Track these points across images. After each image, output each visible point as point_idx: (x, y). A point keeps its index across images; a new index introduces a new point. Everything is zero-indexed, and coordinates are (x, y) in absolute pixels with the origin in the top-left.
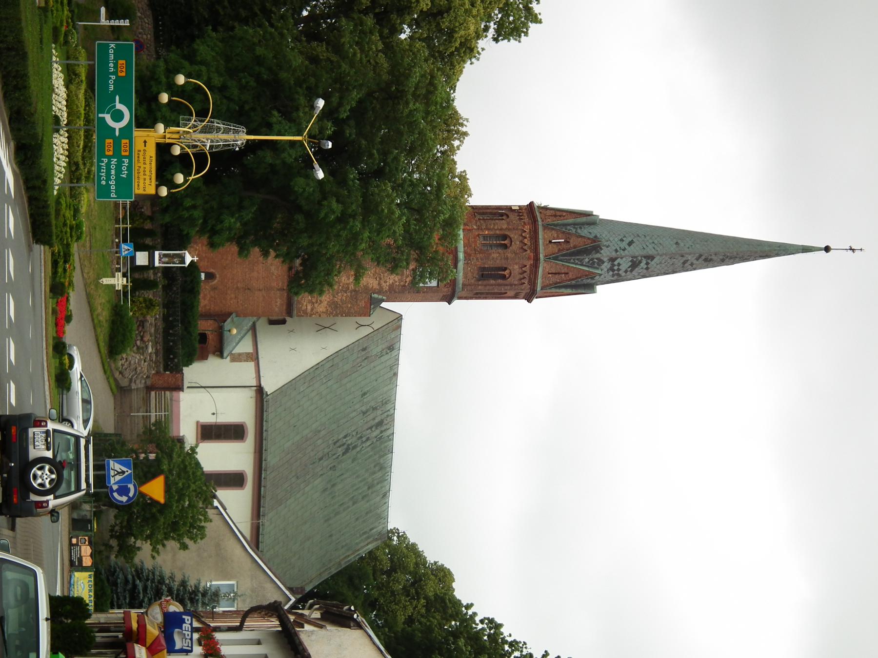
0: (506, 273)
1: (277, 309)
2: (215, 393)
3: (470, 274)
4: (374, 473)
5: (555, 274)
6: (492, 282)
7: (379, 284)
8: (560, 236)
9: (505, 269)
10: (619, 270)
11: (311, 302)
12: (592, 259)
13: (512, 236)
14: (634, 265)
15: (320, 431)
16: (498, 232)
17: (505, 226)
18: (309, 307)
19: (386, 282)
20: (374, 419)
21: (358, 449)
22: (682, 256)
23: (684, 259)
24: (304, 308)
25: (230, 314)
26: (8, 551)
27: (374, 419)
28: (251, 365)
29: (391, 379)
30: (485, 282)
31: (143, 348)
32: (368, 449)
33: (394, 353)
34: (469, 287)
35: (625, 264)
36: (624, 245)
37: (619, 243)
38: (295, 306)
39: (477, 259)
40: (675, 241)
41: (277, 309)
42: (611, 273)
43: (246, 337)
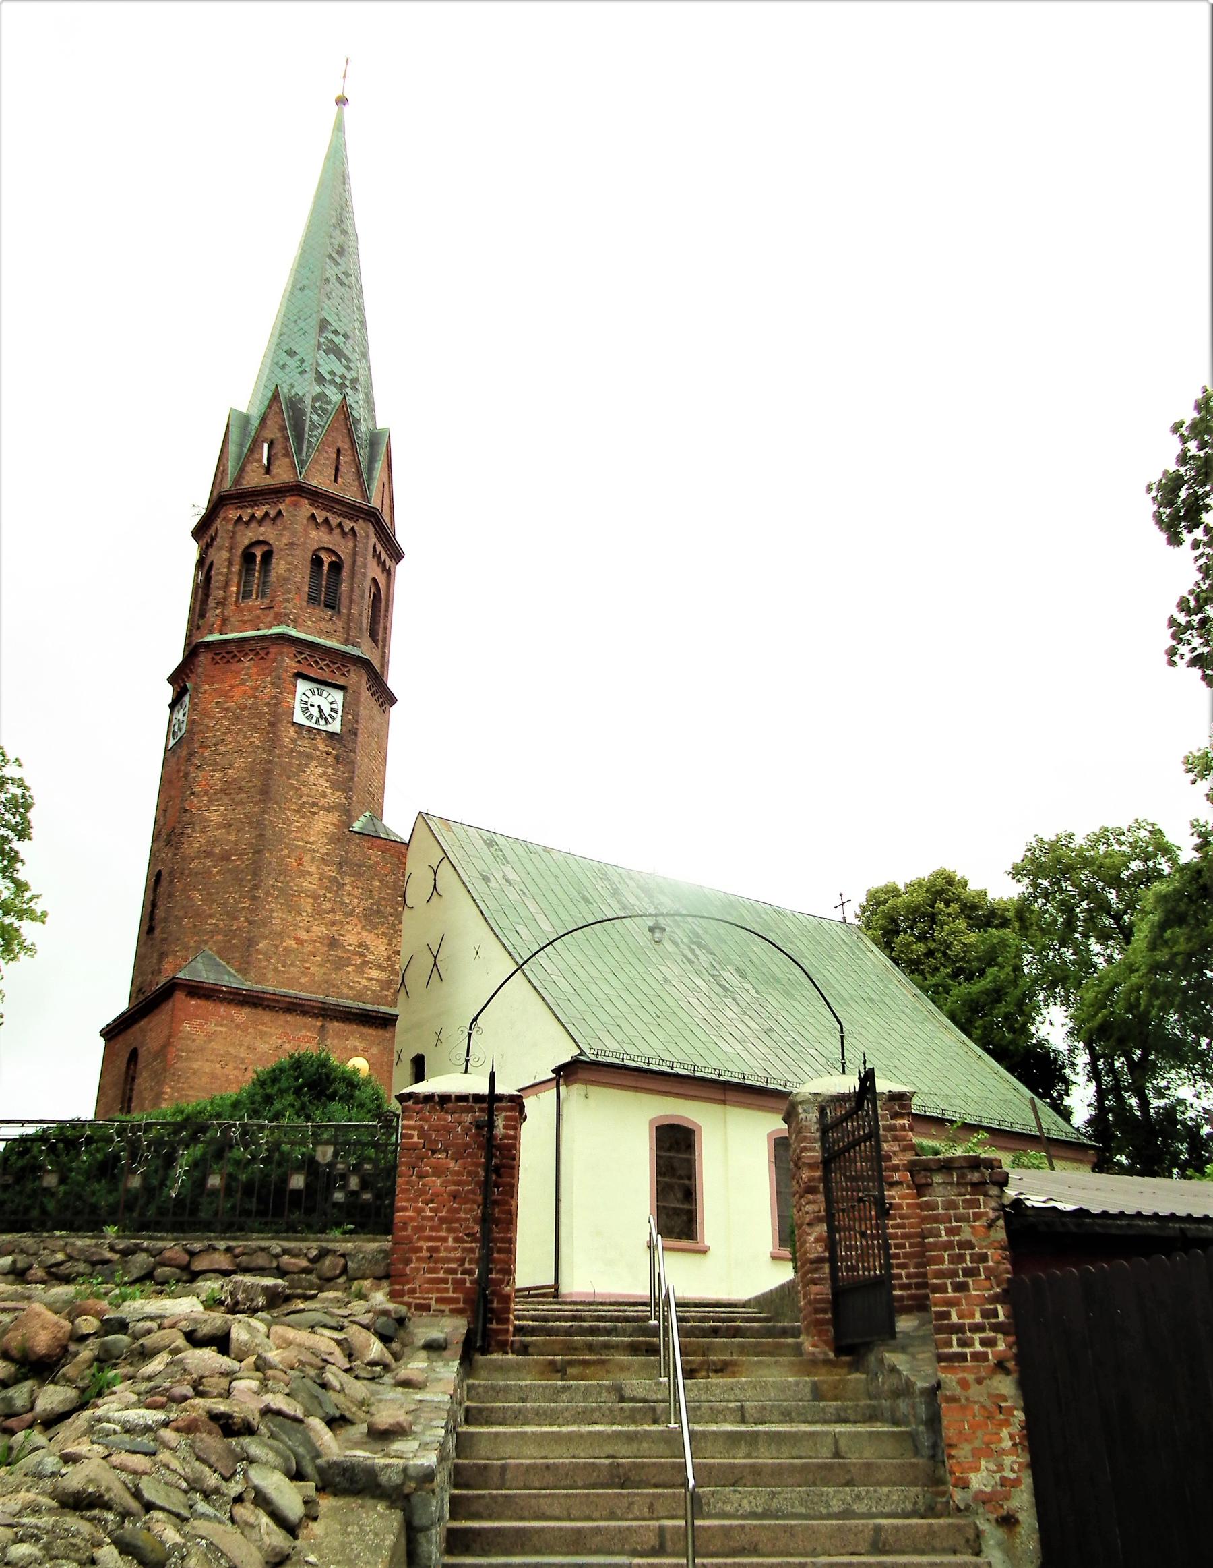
0: (327, 559)
5: (337, 470)
6: (344, 587)
7: (328, 809)
10: (343, 377)
12: (313, 407)
13: (247, 542)
14: (335, 351)
16: (235, 568)
17: (225, 555)
18: (375, 974)
23: (333, 279)
24: (375, 986)
30: (344, 600)
33: (501, 841)
34: (353, 633)
35: (329, 365)
37: (287, 370)
38: (369, 1007)
39: (286, 600)
40: (298, 292)
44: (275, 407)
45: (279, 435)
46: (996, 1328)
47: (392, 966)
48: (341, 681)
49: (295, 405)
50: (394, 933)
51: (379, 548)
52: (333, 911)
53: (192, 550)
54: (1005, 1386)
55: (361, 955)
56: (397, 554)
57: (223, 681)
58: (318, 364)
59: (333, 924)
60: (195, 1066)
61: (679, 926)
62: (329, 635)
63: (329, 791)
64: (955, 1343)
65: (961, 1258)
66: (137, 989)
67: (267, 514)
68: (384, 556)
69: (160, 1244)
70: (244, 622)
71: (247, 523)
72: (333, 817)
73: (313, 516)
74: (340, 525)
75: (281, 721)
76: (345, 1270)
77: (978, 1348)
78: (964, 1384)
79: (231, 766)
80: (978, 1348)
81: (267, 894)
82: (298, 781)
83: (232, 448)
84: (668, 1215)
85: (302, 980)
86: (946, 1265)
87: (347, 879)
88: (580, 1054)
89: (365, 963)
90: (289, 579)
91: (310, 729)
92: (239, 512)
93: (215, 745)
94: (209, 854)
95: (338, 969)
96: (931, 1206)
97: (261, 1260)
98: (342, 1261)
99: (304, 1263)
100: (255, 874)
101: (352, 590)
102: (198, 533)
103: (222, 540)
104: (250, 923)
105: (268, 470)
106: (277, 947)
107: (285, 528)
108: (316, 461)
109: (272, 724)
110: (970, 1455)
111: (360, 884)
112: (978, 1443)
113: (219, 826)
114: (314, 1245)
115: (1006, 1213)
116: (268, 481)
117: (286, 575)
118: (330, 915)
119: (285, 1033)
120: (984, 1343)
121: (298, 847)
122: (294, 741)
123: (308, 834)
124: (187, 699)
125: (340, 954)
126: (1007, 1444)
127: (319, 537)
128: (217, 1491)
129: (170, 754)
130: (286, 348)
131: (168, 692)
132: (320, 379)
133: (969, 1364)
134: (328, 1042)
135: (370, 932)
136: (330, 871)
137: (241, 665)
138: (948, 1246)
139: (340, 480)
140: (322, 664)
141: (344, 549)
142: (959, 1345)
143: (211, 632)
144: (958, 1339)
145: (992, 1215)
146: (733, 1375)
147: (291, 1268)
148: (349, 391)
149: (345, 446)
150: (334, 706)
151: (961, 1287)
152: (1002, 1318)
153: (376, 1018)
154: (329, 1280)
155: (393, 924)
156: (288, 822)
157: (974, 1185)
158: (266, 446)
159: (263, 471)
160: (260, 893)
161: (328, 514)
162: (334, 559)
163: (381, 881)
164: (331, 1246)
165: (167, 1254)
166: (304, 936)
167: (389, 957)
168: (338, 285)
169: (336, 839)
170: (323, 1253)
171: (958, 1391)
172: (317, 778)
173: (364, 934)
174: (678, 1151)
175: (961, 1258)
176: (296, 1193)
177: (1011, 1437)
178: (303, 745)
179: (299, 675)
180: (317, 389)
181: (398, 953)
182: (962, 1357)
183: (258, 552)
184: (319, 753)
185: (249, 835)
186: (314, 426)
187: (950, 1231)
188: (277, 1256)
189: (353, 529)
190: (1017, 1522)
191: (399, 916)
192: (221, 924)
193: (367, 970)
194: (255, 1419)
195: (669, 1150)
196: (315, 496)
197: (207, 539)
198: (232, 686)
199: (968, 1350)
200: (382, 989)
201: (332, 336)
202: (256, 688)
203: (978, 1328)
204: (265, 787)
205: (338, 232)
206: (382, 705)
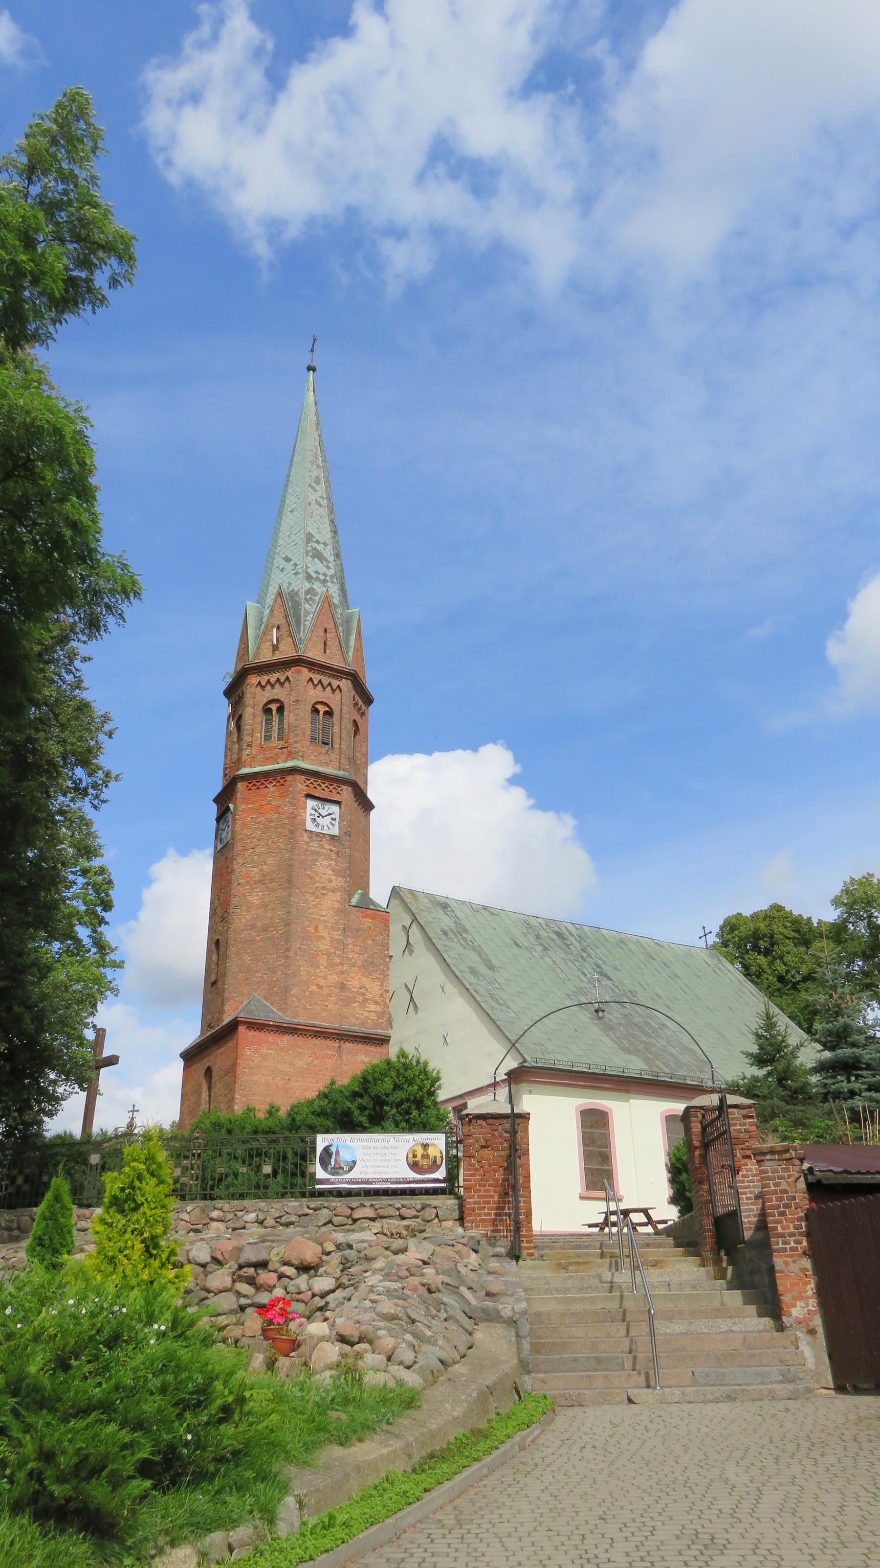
0: (322, 709)
3: (322, 757)
4: (630, 950)
6: (336, 729)
7: (333, 891)
8: (268, 638)
9: (315, 711)
10: (325, 575)
12: (306, 599)
13: (265, 701)
17: (259, 735)
18: (373, 1007)
19: (330, 881)
20: (553, 940)
21: (600, 962)
23: (313, 503)
24: (373, 1016)
29: (492, 914)
30: (337, 740)
31: (345, 1265)
32: (598, 952)
33: (452, 904)
36: (289, 567)
37: (285, 572)
38: (370, 1031)
39: (296, 742)
45: (284, 621)
46: (801, 1234)
49: (294, 595)
50: (384, 978)
51: (357, 698)
54: (807, 1263)
55: (364, 994)
58: (307, 567)
60: (255, 1078)
63: (333, 878)
65: (781, 1199)
66: (207, 1024)
68: (360, 703)
69: (334, 1204)
70: (268, 759)
73: (311, 679)
74: (330, 684)
75: (297, 829)
77: (793, 1244)
80: (793, 1244)
81: (296, 954)
84: (592, 1175)
85: (324, 1015)
86: (774, 1203)
87: (350, 941)
89: (365, 1000)
90: (296, 727)
91: (318, 834)
92: (258, 679)
94: (253, 927)
96: (766, 1172)
97: (392, 1211)
98: (435, 1211)
100: (287, 941)
102: (228, 693)
103: (248, 699)
104: (286, 975)
106: (305, 991)
109: (292, 832)
112: (795, 1293)
114: (418, 1202)
115: (805, 1174)
116: (278, 656)
117: (296, 723)
119: (314, 1053)
120: (796, 1242)
122: (307, 843)
123: (321, 910)
125: (347, 994)
126: (810, 1293)
127: (316, 694)
128: (437, 1316)
130: (283, 556)
131: (214, 809)
132: (309, 578)
134: (344, 1057)
136: (337, 935)
138: (775, 1192)
139: (328, 651)
140: (323, 786)
141: (334, 701)
143: (245, 767)
145: (797, 1175)
146: (662, 1267)
148: (329, 584)
151: (782, 1214)
155: (383, 971)
157: (787, 1160)
158: (275, 630)
160: (291, 954)
162: (327, 709)
163: (373, 940)
164: (428, 1202)
165: (339, 1210)
166: (322, 982)
167: (382, 995)
168: (317, 507)
169: (341, 912)
172: (326, 870)
173: (364, 979)
174: (597, 1128)
177: (812, 1289)
178: (314, 846)
179: (308, 796)
180: (307, 586)
182: (785, 1250)
183: (274, 707)
184: (325, 851)
186: (307, 613)
187: (776, 1185)
188: (398, 1209)
189: (339, 687)
190: (816, 1332)
191: (386, 965)
193: (367, 1005)
194: (440, 1285)
195: (591, 1127)
196: (312, 665)
198: (262, 806)
201: (315, 545)
203: (792, 1235)
204: (287, 878)
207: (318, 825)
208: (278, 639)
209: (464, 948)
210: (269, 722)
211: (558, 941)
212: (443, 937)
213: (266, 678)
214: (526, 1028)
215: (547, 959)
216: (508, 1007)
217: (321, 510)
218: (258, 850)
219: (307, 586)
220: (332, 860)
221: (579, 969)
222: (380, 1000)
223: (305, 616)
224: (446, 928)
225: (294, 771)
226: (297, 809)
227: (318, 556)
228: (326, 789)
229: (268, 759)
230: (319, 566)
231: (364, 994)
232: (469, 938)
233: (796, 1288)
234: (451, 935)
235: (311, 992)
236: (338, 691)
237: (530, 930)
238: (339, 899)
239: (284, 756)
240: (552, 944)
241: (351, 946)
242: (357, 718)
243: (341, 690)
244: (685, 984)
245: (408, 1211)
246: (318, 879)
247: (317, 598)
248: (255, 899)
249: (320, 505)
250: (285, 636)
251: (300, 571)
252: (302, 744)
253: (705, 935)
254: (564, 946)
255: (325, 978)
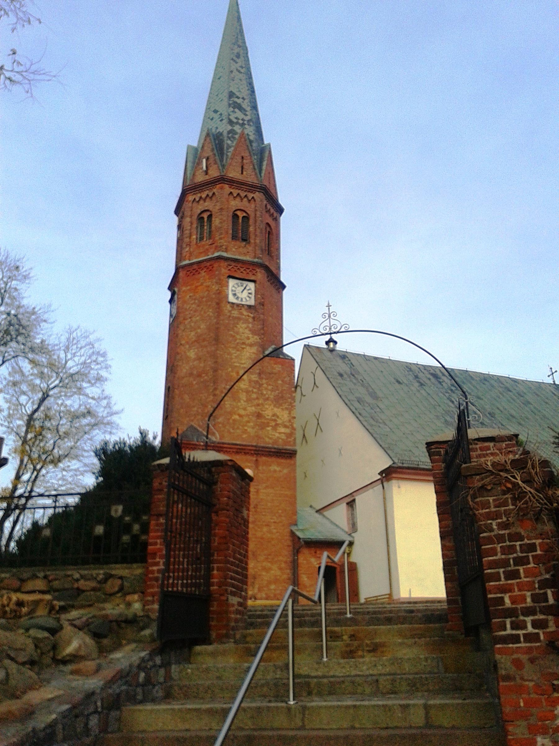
0: (241, 214)
1: (285, 471)
2: (312, 335)
3: (241, 250)
6: (251, 229)
7: (251, 345)
9: (235, 216)
10: (243, 120)
11: (275, 428)
13: (199, 212)
15: (446, 421)
16: (195, 226)
18: (282, 430)
19: (248, 338)
20: (429, 379)
22: (232, 72)
23: (235, 71)
24: (283, 437)
25: (293, 534)
26: (259, 648)
27: (429, 379)
28: (358, 499)
30: (252, 236)
36: (216, 116)
37: (214, 120)
38: (281, 447)
39: (221, 239)
41: (285, 471)
42: (246, 126)
43: (328, 517)
44: (208, 140)
46: (547, 610)
47: (292, 425)
48: (253, 278)
50: (291, 408)
52: (257, 398)
53: (175, 220)
55: (275, 420)
56: (280, 210)
57: (192, 285)
58: (229, 115)
59: (258, 405)
61: (454, 392)
62: (245, 254)
63: (250, 336)
64: (508, 626)
67: (208, 195)
68: (272, 211)
70: (201, 253)
71: (198, 202)
72: (254, 349)
74: (246, 196)
76: (121, 589)
77: (530, 629)
78: (518, 664)
79: (199, 328)
80: (530, 629)
82: (234, 332)
83: (189, 165)
86: (499, 556)
87: (264, 381)
88: (393, 463)
89: (277, 425)
91: (238, 305)
92: (194, 197)
93: (190, 318)
94: (191, 374)
95: (262, 429)
98: (119, 582)
99: (93, 584)
101: (255, 230)
103: (188, 213)
105: (206, 173)
106: (229, 419)
107: (217, 202)
108: (230, 164)
109: (218, 304)
110: (526, 732)
111: (271, 383)
113: (195, 360)
114: (101, 572)
117: (220, 225)
118: (257, 401)
121: (236, 366)
122: (230, 311)
123: (241, 359)
124: (176, 296)
125: (263, 420)
127: (235, 204)
129: (171, 325)
132: (231, 122)
133: (523, 645)
134: (260, 468)
135: (278, 408)
137: (200, 275)
138: (500, 539)
139: (244, 173)
140: (242, 270)
141: (250, 208)
142: (512, 628)
143: (185, 260)
144: (512, 623)
147: (85, 588)
149: (246, 154)
150: (250, 291)
151: (514, 575)
152: (551, 601)
153: (285, 453)
154: (111, 595)
155: (291, 403)
156: (229, 354)
158: (204, 160)
159: (204, 173)
161: (239, 191)
162: (245, 214)
163: (283, 381)
164: (113, 572)
166: (242, 412)
167: (290, 421)
168: (238, 73)
170: (109, 576)
171: (512, 670)
172: (244, 331)
173: (275, 409)
175: (512, 549)
176: (98, 538)
178: (235, 313)
180: (229, 128)
181: (294, 418)
182: (515, 639)
183: (205, 216)
184: (244, 317)
185: (210, 363)
186: (229, 147)
189: (253, 198)
192: (200, 411)
196: (232, 182)
197: (181, 215)
198: (197, 287)
199: (521, 632)
200: (287, 437)
201: (236, 100)
202: (208, 286)
203: (528, 612)
205: (236, 47)
206: (278, 289)
207: (237, 298)
208: (207, 167)
209: (355, 384)
210: (202, 226)
211: (433, 380)
212: (339, 377)
213: (199, 195)
214: (251, 370)
215: (423, 392)
216: (385, 424)
217: (241, 75)
218: (194, 319)
219: (229, 128)
220: (249, 323)
221: (448, 399)
222: (288, 424)
223: (228, 149)
224: (342, 372)
225: (219, 258)
226: (222, 287)
227: (240, 108)
228: (244, 272)
229: (201, 253)
230: (239, 114)
231: (275, 420)
232: (360, 378)
233: (534, 710)
234: (345, 376)
235: (234, 420)
236: (252, 201)
237: (411, 373)
238: (255, 351)
239: (213, 250)
240: (428, 381)
241: (265, 385)
242: (270, 221)
243: (255, 201)
244: (535, 408)
245: (88, 583)
246: (238, 337)
247: (237, 136)
248: (192, 354)
249: (239, 72)
250: (212, 164)
251: (224, 118)
252: (224, 239)
253: (553, 374)
254: (437, 383)
255: (245, 409)
